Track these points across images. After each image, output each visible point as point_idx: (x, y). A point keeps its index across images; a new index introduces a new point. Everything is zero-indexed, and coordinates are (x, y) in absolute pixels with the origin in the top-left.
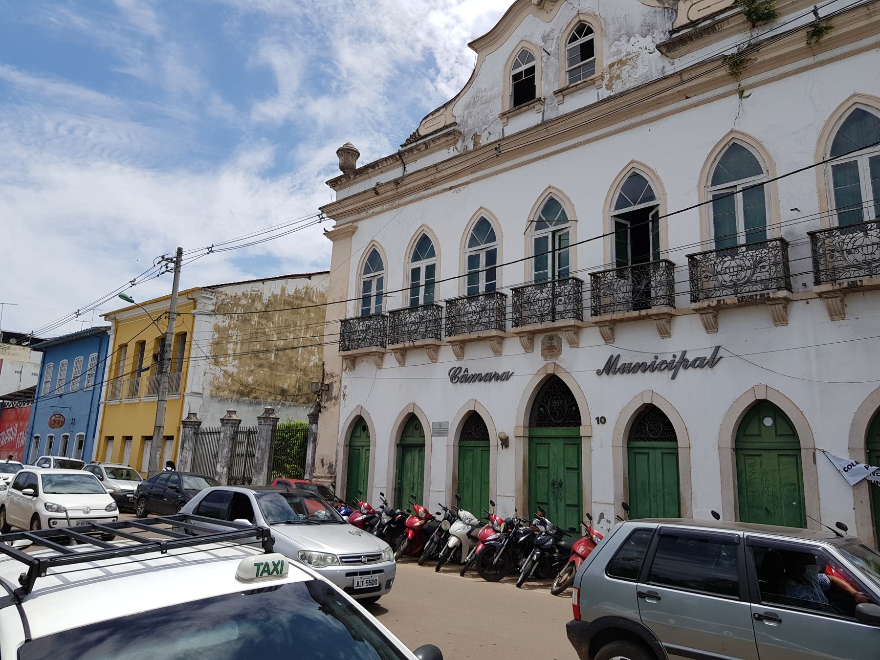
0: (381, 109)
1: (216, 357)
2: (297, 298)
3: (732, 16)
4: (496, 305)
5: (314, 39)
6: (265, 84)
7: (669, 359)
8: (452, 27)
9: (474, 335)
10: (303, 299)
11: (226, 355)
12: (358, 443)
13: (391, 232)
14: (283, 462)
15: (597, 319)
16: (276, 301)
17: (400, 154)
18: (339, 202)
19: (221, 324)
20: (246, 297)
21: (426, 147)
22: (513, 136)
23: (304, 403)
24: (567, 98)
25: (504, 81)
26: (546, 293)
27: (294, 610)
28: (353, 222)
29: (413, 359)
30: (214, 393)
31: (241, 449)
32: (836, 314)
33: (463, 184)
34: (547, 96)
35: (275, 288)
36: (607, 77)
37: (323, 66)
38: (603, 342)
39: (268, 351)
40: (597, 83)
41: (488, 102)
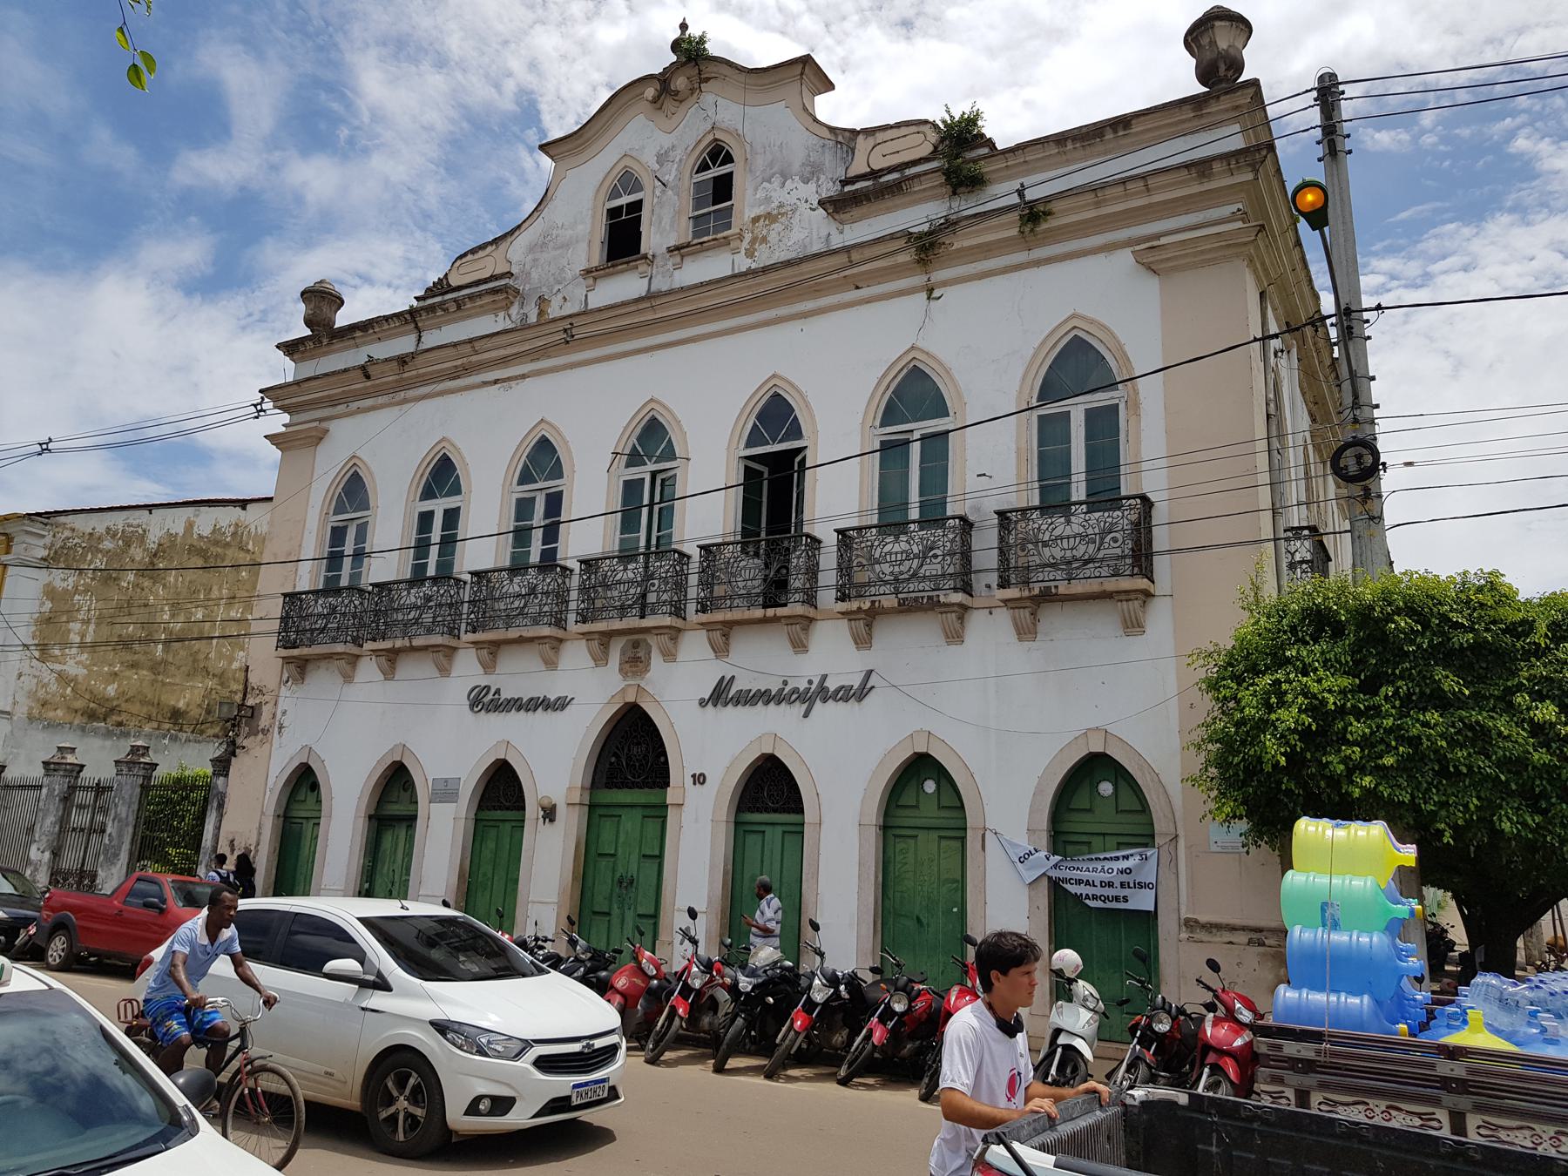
0: (432, 191)
1: (43, 648)
2: (216, 543)
3: (926, 173)
4: (553, 585)
5: (310, 44)
6: (205, 117)
7: (803, 686)
8: (574, 60)
9: (513, 633)
10: (227, 545)
11: (66, 644)
12: (299, 812)
13: (388, 445)
14: (163, 844)
15: (704, 618)
16: (173, 544)
17: (412, 312)
18: (297, 383)
19: (59, 584)
20: (114, 536)
21: (459, 308)
22: (599, 310)
23: (216, 736)
24: (687, 260)
25: (593, 217)
26: (633, 571)
27: (90, 1065)
28: (321, 420)
29: (409, 668)
30: (36, 712)
31: (79, 819)
32: (1026, 632)
33: (516, 378)
34: (658, 252)
35: (175, 522)
36: (748, 237)
37: (323, 96)
38: (712, 655)
39: (149, 640)
40: (733, 245)
41: (565, 246)
